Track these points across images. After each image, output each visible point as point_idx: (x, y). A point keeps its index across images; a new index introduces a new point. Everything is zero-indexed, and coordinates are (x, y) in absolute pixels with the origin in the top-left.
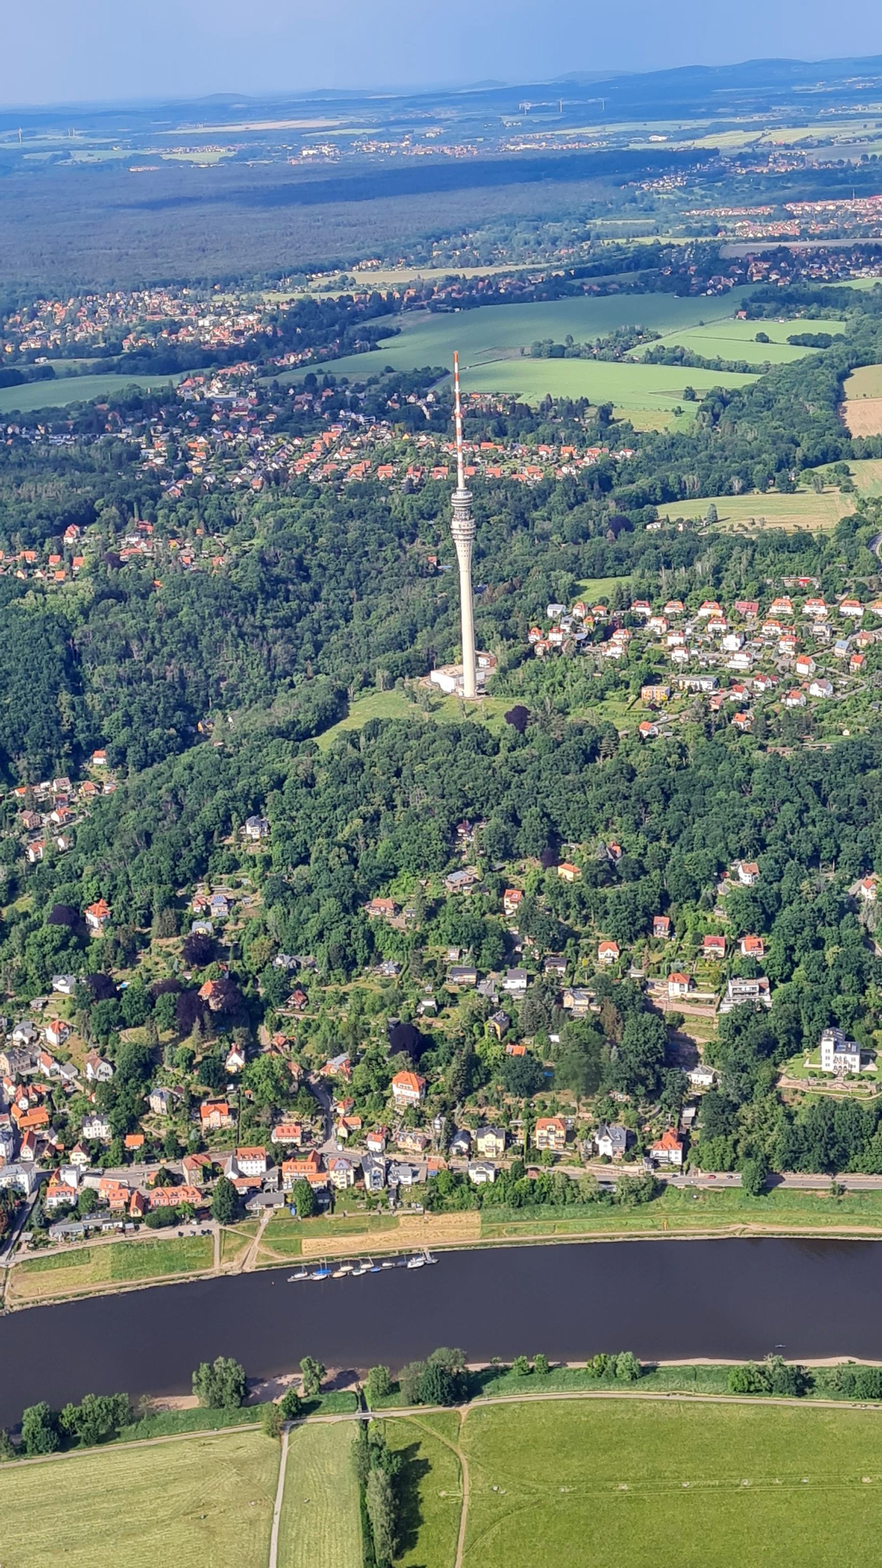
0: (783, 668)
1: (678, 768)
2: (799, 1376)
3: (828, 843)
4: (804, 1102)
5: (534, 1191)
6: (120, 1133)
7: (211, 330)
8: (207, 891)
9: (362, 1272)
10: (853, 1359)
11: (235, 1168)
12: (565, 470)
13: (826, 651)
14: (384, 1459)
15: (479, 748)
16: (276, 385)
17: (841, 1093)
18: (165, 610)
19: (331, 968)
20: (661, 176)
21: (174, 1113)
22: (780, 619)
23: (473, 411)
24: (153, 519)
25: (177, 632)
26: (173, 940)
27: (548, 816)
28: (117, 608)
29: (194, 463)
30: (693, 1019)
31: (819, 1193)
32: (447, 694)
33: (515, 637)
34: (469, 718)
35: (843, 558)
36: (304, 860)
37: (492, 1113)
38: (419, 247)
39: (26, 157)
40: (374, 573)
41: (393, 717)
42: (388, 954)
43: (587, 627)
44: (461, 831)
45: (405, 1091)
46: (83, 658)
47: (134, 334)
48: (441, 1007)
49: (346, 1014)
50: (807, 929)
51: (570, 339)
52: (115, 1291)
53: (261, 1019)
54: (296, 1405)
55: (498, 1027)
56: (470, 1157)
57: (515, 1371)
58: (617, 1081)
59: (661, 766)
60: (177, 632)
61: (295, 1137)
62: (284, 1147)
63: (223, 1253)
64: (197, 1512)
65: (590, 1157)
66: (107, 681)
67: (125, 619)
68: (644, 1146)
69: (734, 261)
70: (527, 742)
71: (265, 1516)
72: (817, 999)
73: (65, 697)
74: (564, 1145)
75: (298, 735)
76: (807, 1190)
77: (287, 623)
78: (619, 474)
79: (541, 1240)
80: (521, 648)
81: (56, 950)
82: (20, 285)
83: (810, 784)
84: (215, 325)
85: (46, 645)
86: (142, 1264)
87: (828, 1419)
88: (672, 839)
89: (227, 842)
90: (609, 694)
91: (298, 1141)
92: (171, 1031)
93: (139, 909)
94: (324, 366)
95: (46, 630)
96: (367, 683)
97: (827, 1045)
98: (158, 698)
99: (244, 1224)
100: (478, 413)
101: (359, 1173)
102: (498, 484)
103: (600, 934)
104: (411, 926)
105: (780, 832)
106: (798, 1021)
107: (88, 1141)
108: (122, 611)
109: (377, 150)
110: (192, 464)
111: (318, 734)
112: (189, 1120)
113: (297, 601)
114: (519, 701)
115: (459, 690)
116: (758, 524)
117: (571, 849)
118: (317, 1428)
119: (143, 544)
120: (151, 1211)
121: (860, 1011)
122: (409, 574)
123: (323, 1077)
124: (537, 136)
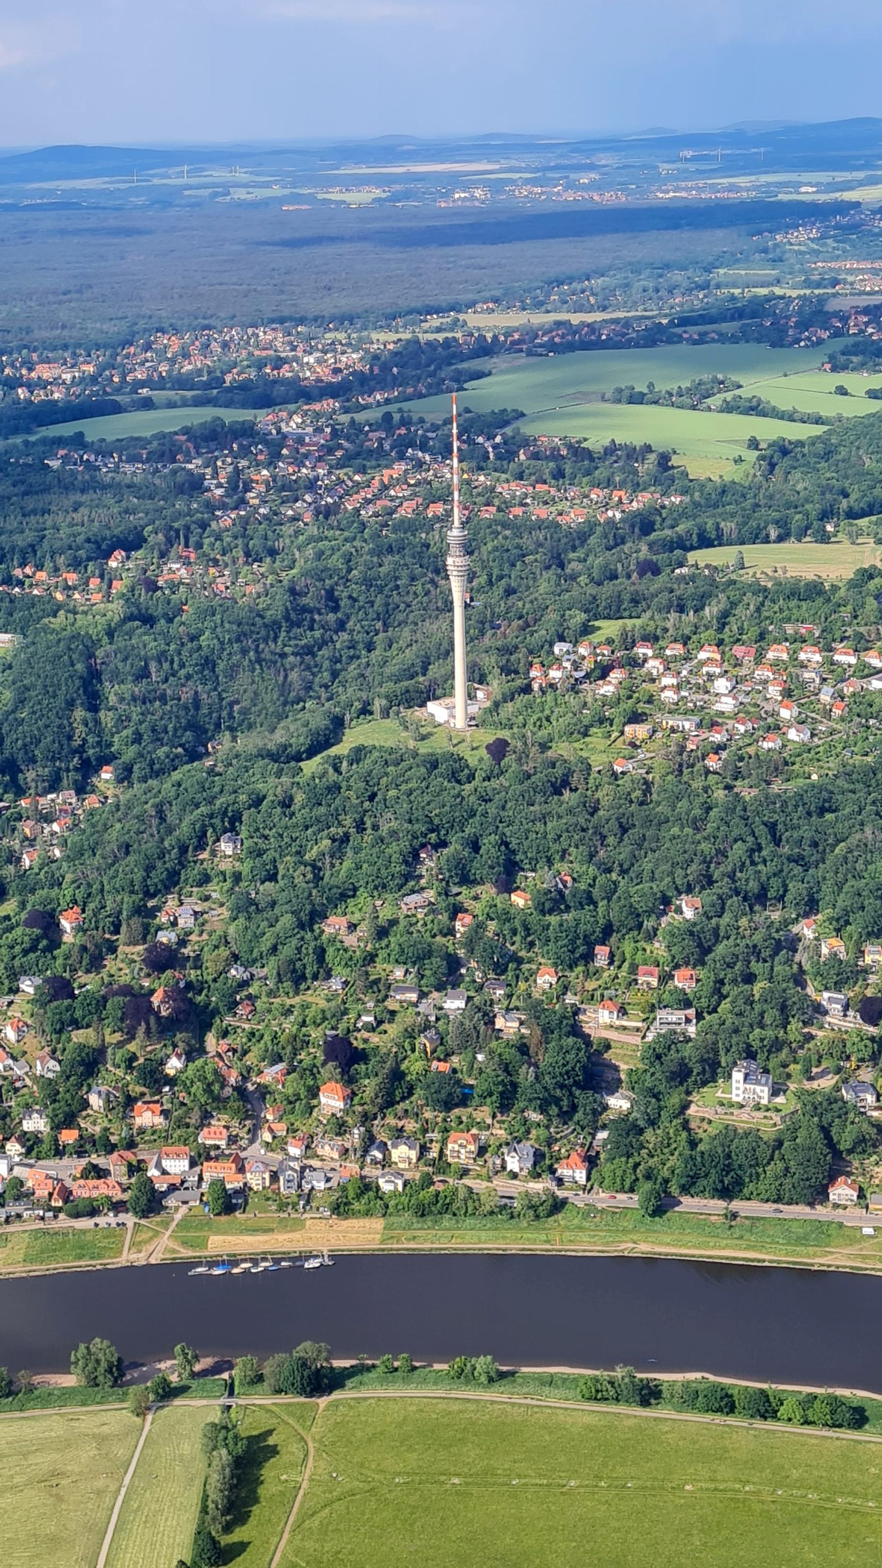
0: (766, 712)
1: (642, 804)
2: (647, 1386)
3: (775, 883)
4: (710, 1129)
5: (437, 1202)
6: (57, 1127)
7: (313, 367)
8: (176, 902)
9: (260, 1269)
10: (706, 1375)
11: (158, 1165)
12: (610, 513)
13: (812, 698)
14: (230, 1441)
15: (453, 776)
16: (353, 421)
17: (747, 1122)
18: (188, 635)
19: (280, 981)
20: (797, 227)
21: (110, 1110)
22: (776, 665)
23: (537, 453)
24: (199, 546)
25: (195, 656)
26: (140, 948)
27: (507, 844)
28: (142, 630)
29: (252, 495)
30: (618, 1045)
31: (713, 1218)
32: (439, 725)
33: (516, 672)
34: (456, 749)
35: (849, 608)
36: (272, 877)
37: (411, 1126)
38: (539, 291)
39: (186, 193)
40: (402, 606)
41: (377, 745)
42: (337, 970)
43: (588, 665)
44: (423, 855)
45: (331, 1101)
46: (103, 677)
47: (239, 368)
48: (380, 1022)
49: (289, 1025)
50: (739, 964)
51: (651, 385)
52: (24, 1275)
53: (209, 1026)
54: (164, 1389)
55: (428, 1045)
56: (384, 1166)
57: (381, 1369)
58: (530, 1100)
59: (622, 801)
60: (195, 656)
61: (221, 1139)
62: (207, 1149)
63: (133, 1244)
64: (50, 1481)
65: (497, 1173)
66: (122, 700)
67: (148, 642)
68: (552, 1165)
69: (836, 314)
70: (502, 773)
71: (112, 1488)
72: (736, 1031)
73: (79, 713)
74: (475, 1159)
75: (286, 757)
76: (701, 1214)
77: (309, 651)
78: (664, 520)
79: (437, 1249)
80: (519, 682)
81: (25, 952)
82: (144, 317)
83: (765, 825)
84: (319, 361)
85: (68, 663)
86: (55, 1250)
87: (667, 1429)
88: (623, 872)
89: (201, 857)
90: (593, 730)
91: (223, 1143)
92: (120, 1034)
93: (109, 916)
94: (405, 406)
95: (70, 649)
96: (365, 711)
97: (737, 1076)
98: (170, 718)
99: (158, 1219)
100: (541, 455)
101: (274, 1177)
102: (540, 525)
103: (542, 961)
104: (362, 945)
105: (729, 869)
106: (716, 1052)
107: (26, 1133)
108: (145, 634)
109: (529, 196)
110: (250, 495)
111: (309, 758)
112: (123, 1118)
113: (322, 631)
114: (505, 734)
115: (452, 721)
116: (780, 572)
117: (527, 878)
118: (180, 1411)
119: (183, 571)
120: (72, 1201)
121: (777, 1045)
122: (437, 608)
123: (259, 1084)
124: (690, 184)
